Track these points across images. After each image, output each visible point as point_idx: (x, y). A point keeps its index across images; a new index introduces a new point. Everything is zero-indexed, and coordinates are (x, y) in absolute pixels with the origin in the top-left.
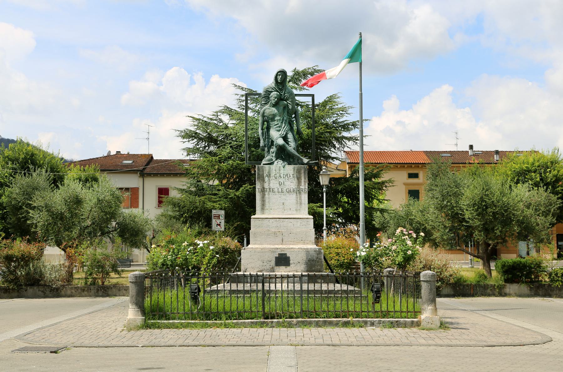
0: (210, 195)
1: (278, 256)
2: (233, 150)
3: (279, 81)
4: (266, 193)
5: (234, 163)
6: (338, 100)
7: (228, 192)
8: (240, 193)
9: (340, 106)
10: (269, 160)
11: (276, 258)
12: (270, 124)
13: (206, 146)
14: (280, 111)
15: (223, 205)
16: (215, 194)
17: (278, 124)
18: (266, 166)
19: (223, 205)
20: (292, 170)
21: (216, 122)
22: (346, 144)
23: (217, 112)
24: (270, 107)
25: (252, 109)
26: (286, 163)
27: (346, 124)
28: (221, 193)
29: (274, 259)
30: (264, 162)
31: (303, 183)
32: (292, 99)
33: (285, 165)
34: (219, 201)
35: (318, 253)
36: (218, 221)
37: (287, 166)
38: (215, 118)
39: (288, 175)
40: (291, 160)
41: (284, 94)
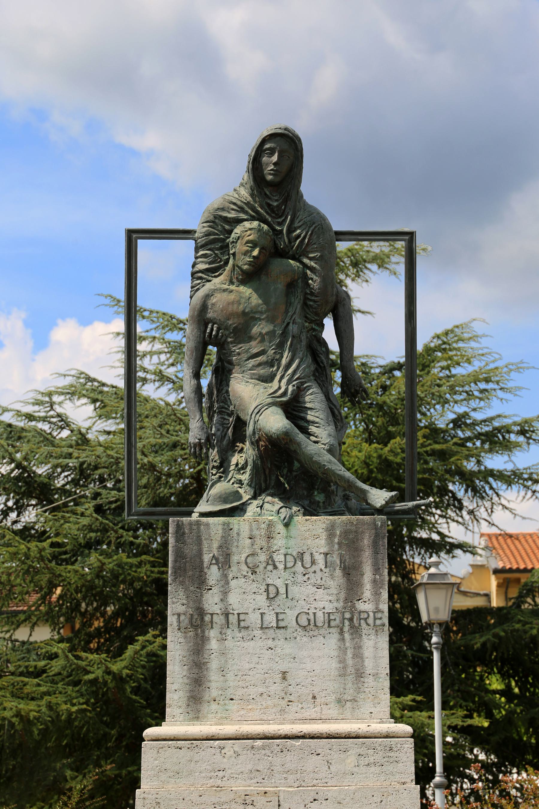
0: (21, 674)
2: (107, 519)
3: (269, 178)
4: (213, 633)
5: (106, 561)
6: (473, 344)
7: (84, 663)
8: (124, 664)
9: (477, 365)
10: (224, 498)
12: (231, 353)
13: (11, 509)
14: (273, 300)
15: (64, 707)
16: (38, 673)
17: (262, 353)
18: (211, 520)
19: (64, 707)
20: (324, 536)
21: (46, 427)
22: (498, 495)
23: (50, 394)
24: (231, 282)
25: (174, 382)
26: (295, 509)
27: (498, 430)
28: (57, 665)
30: (203, 507)
31: (367, 592)
32: (321, 249)
33: (291, 517)
34: (48, 693)
37: (300, 519)
38: (42, 414)
39: (307, 558)
40: (320, 497)
41: (290, 230)
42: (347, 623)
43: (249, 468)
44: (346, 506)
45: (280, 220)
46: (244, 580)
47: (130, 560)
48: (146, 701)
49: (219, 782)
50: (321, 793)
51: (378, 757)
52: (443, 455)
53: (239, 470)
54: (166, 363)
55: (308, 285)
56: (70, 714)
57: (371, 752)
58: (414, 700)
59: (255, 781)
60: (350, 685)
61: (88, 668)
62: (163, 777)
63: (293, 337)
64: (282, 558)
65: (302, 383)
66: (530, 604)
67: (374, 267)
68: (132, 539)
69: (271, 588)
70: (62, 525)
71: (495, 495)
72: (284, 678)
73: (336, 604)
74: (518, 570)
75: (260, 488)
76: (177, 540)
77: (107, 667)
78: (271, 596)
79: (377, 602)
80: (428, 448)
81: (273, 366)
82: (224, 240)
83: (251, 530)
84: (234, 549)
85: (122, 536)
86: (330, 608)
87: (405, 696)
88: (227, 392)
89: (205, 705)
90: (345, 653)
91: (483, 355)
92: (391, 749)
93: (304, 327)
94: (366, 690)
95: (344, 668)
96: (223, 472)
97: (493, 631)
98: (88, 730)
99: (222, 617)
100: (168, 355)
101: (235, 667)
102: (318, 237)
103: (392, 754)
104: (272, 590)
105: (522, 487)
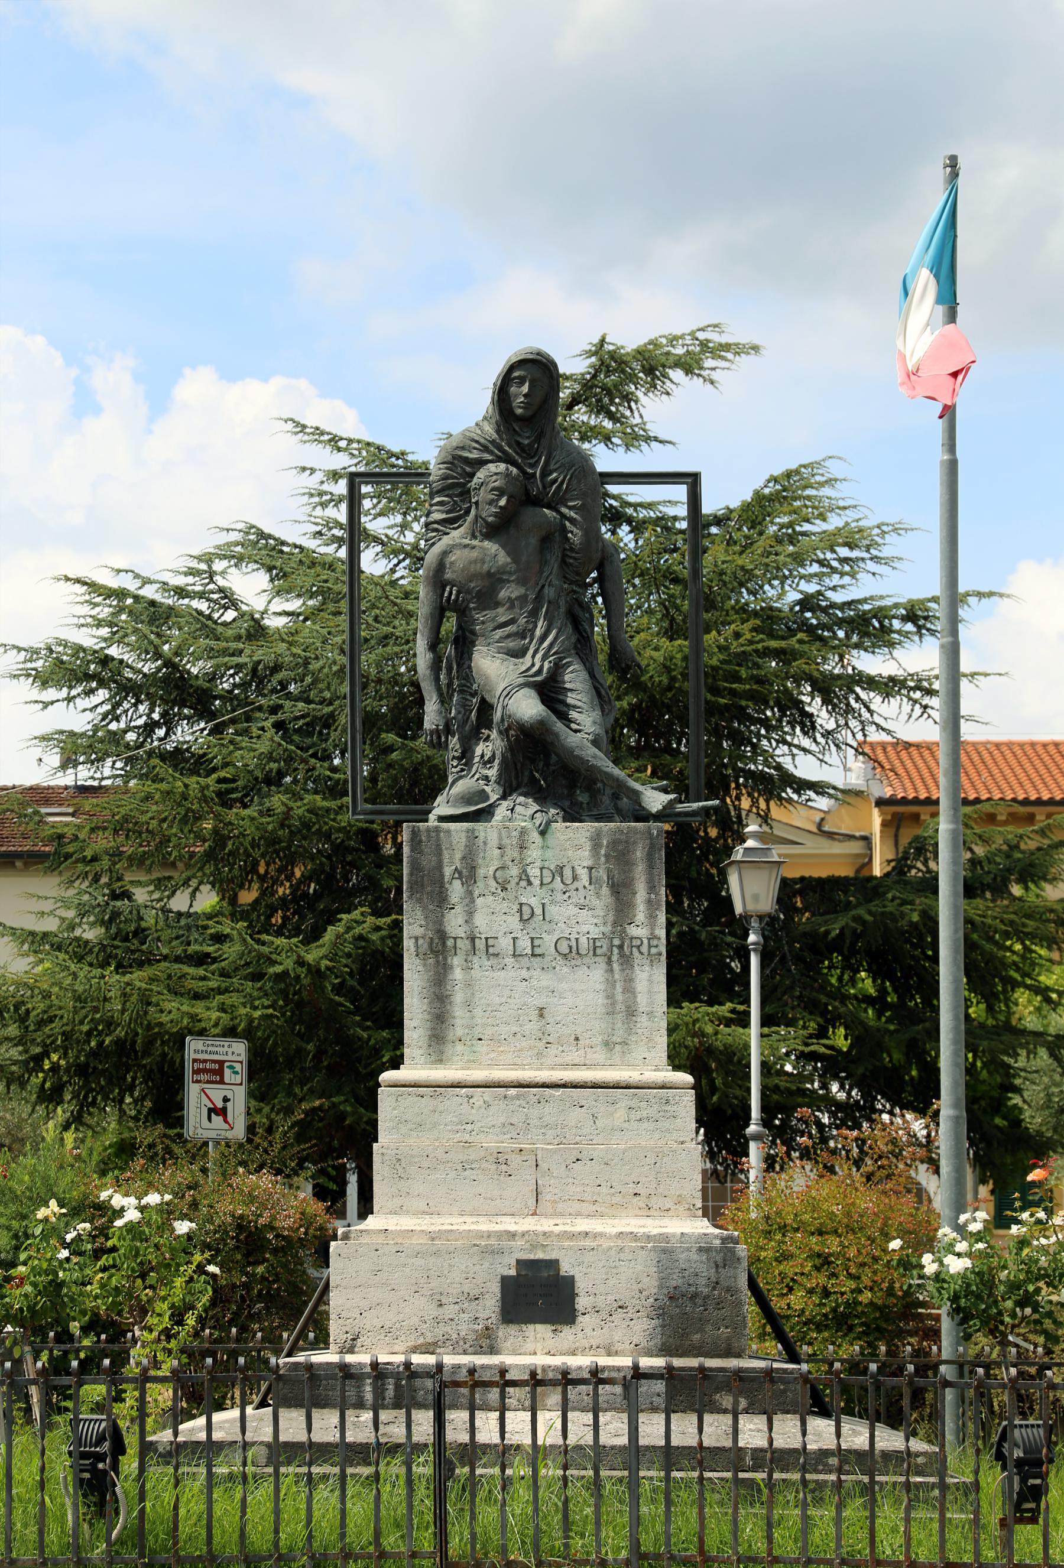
1: (513, 1272)
3: (519, 411)
4: (456, 961)
6: (826, 491)
8: (323, 951)
9: (834, 522)
10: (468, 799)
11: (505, 1281)
12: (474, 621)
13: (157, 724)
14: (524, 558)
15: (243, 1011)
16: (202, 959)
18: (452, 826)
19: (243, 1011)
20: (588, 846)
21: (203, 606)
24: (474, 537)
25: (383, 543)
26: (553, 811)
28: (231, 951)
29: (495, 1288)
30: (442, 806)
31: (641, 913)
32: (583, 496)
33: (548, 823)
35: (719, 1258)
36: (217, 1095)
37: (559, 826)
38: (198, 588)
39: (568, 873)
40: (583, 798)
41: (545, 473)
42: (616, 951)
43: (497, 762)
44: (616, 807)
45: (532, 461)
46: (492, 898)
47: (326, 804)
48: (353, 1003)
49: (467, 1137)
50: (585, 1152)
51: (652, 1111)
52: (784, 656)
53: (485, 763)
54: (373, 512)
55: (568, 539)
56: (251, 1020)
57: (644, 1104)
58: (733, 1011)
59: (509, 1136)
60: (620, 1025)
61: (274, 956)
62: (404, 1129)
63: (549, 602)
64: (537, 872)
65: (561, 659)
66: (919, 870)
67: (677, 375)
68: (328, 773)
69: (525, 908)
70: (232, 752)
71: (863, 710)
72: (541, 1016)
73: (602, 929)
74: (916, 801)
75: (511, 786)
76: (413, 849)
77: (299, 956)
78: (525, 917)
79: (652, 926)
80: (760, 646)
81: (525, 638)
82: (464, 485)
83: (500, 838)
84: (480, 861)
85: (314, 768)
86: (595, 933)
87: (721, 1004)
88: (470, 667)
89: (450, 1046)
90: (614, 987)
91: (845, 508)
92: (667, 1102)
93: (562, 588)
94: (640, 1031)
95: (613, 1004)
96: (465, 765)
97: (854, 912)
98: (275, 1044)
99: (467, 942)
100: (375, 501)
101: (483, 1001)
102: (579, 482)
103: (669, 1108)
104: (526, 911)
105: (905, 700)
